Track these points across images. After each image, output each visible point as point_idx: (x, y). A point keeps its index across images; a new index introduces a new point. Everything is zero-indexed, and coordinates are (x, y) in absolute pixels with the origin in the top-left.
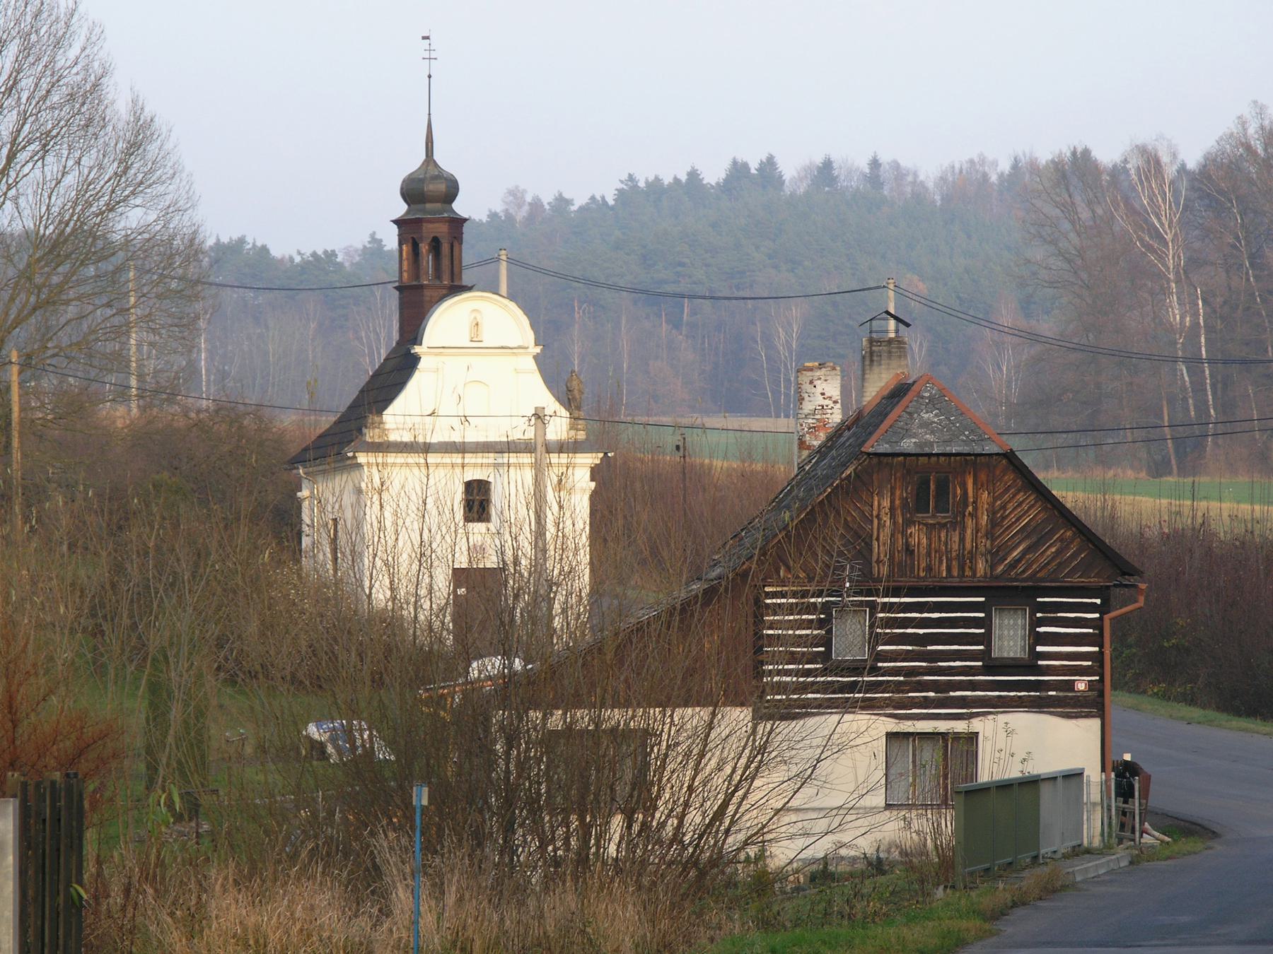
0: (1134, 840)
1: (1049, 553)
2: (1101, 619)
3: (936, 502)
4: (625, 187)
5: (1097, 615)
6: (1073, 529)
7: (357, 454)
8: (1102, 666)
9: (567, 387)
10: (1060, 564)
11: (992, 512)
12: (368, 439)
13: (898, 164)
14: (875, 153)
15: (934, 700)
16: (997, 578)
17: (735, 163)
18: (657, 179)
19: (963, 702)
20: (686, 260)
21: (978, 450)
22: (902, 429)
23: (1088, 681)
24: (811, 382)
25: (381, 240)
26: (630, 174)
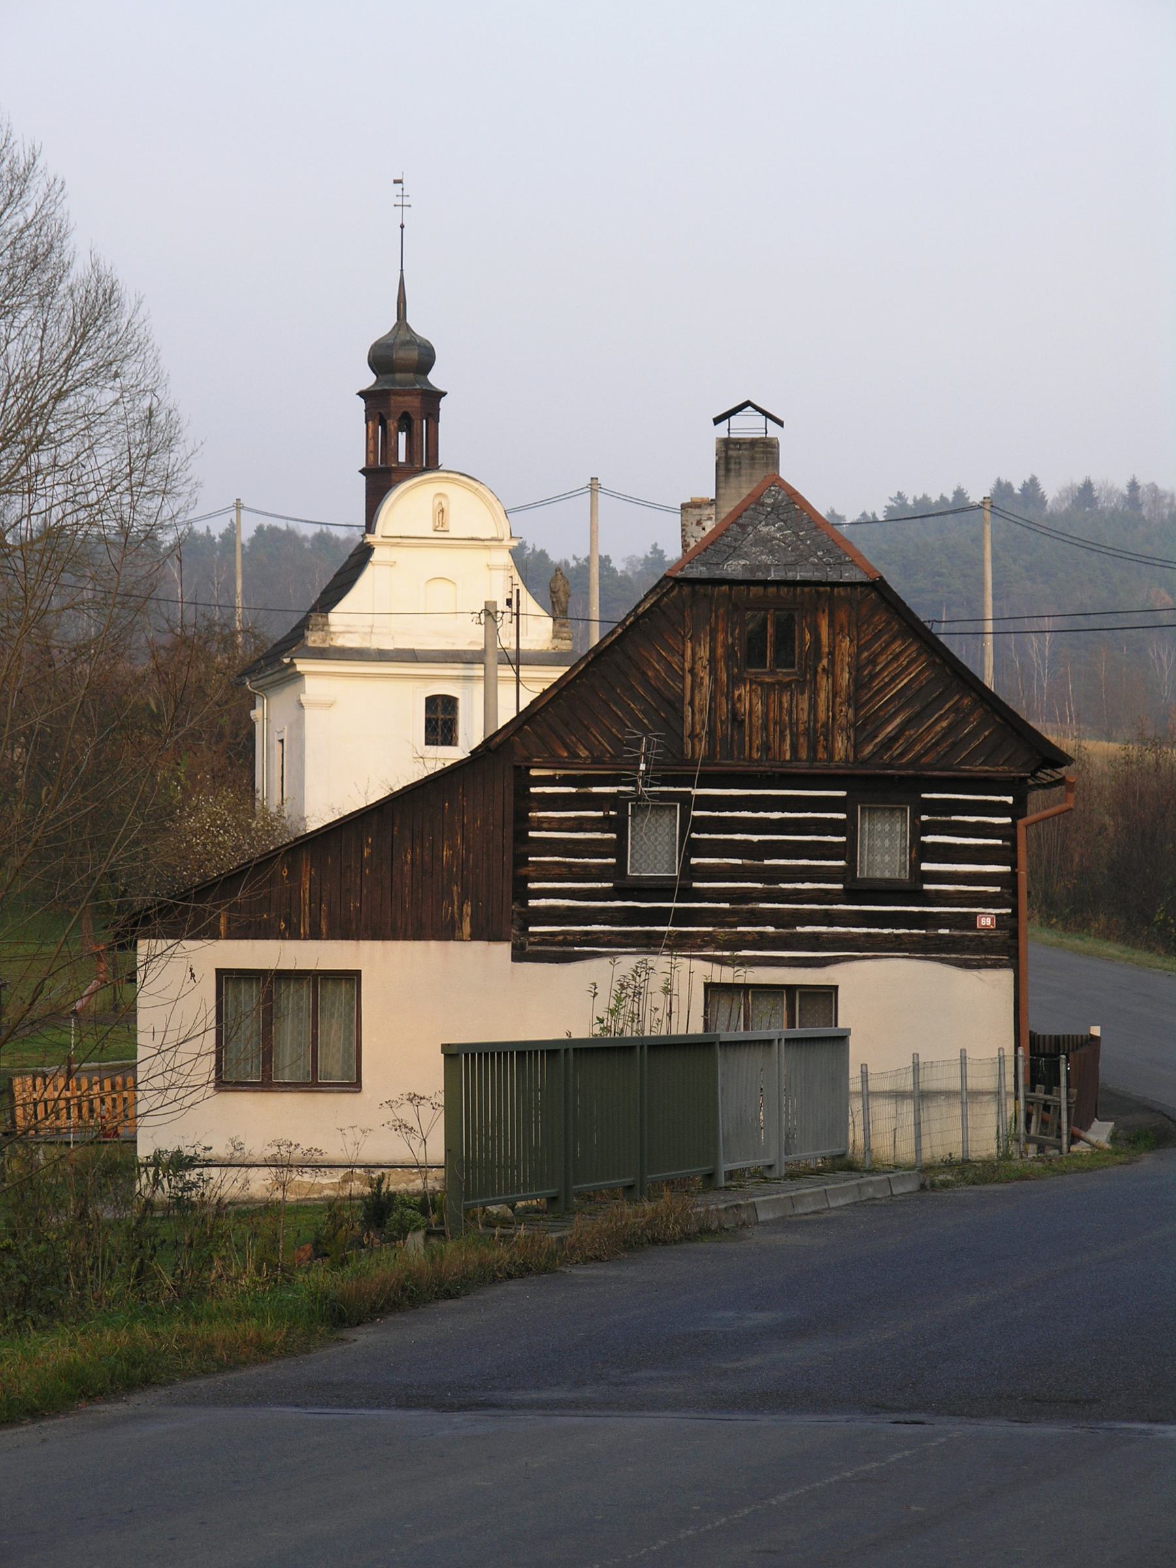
0: (1060, 1148)
1: (938, 728)
2: (1013, 825)
3: (777, 651)
4: (895, 505)
5: (1008, 820)
6: (973, 695)
7: (295, 661)
8: (1015, 894)
9: (551, 588)
10: (954, 744)
11: (856, 669)
12: (310, 644)
13: (1156, 487)
14: (1134, 476)
15: (774, 937)
16: (864, 762)
17: (999, 482)
18: (925, 498)
19: (815, 942)
20: (944, 571)
21: (833, 576)
22: (729, 547)
23: (997, 915)
24: (699, 523)
25: (663, 551)
26: (899, 493)
